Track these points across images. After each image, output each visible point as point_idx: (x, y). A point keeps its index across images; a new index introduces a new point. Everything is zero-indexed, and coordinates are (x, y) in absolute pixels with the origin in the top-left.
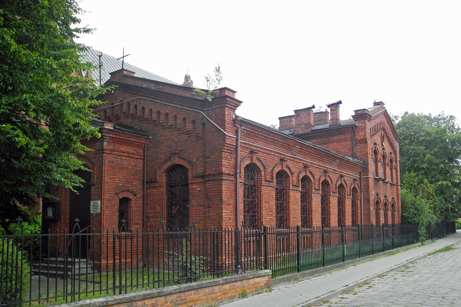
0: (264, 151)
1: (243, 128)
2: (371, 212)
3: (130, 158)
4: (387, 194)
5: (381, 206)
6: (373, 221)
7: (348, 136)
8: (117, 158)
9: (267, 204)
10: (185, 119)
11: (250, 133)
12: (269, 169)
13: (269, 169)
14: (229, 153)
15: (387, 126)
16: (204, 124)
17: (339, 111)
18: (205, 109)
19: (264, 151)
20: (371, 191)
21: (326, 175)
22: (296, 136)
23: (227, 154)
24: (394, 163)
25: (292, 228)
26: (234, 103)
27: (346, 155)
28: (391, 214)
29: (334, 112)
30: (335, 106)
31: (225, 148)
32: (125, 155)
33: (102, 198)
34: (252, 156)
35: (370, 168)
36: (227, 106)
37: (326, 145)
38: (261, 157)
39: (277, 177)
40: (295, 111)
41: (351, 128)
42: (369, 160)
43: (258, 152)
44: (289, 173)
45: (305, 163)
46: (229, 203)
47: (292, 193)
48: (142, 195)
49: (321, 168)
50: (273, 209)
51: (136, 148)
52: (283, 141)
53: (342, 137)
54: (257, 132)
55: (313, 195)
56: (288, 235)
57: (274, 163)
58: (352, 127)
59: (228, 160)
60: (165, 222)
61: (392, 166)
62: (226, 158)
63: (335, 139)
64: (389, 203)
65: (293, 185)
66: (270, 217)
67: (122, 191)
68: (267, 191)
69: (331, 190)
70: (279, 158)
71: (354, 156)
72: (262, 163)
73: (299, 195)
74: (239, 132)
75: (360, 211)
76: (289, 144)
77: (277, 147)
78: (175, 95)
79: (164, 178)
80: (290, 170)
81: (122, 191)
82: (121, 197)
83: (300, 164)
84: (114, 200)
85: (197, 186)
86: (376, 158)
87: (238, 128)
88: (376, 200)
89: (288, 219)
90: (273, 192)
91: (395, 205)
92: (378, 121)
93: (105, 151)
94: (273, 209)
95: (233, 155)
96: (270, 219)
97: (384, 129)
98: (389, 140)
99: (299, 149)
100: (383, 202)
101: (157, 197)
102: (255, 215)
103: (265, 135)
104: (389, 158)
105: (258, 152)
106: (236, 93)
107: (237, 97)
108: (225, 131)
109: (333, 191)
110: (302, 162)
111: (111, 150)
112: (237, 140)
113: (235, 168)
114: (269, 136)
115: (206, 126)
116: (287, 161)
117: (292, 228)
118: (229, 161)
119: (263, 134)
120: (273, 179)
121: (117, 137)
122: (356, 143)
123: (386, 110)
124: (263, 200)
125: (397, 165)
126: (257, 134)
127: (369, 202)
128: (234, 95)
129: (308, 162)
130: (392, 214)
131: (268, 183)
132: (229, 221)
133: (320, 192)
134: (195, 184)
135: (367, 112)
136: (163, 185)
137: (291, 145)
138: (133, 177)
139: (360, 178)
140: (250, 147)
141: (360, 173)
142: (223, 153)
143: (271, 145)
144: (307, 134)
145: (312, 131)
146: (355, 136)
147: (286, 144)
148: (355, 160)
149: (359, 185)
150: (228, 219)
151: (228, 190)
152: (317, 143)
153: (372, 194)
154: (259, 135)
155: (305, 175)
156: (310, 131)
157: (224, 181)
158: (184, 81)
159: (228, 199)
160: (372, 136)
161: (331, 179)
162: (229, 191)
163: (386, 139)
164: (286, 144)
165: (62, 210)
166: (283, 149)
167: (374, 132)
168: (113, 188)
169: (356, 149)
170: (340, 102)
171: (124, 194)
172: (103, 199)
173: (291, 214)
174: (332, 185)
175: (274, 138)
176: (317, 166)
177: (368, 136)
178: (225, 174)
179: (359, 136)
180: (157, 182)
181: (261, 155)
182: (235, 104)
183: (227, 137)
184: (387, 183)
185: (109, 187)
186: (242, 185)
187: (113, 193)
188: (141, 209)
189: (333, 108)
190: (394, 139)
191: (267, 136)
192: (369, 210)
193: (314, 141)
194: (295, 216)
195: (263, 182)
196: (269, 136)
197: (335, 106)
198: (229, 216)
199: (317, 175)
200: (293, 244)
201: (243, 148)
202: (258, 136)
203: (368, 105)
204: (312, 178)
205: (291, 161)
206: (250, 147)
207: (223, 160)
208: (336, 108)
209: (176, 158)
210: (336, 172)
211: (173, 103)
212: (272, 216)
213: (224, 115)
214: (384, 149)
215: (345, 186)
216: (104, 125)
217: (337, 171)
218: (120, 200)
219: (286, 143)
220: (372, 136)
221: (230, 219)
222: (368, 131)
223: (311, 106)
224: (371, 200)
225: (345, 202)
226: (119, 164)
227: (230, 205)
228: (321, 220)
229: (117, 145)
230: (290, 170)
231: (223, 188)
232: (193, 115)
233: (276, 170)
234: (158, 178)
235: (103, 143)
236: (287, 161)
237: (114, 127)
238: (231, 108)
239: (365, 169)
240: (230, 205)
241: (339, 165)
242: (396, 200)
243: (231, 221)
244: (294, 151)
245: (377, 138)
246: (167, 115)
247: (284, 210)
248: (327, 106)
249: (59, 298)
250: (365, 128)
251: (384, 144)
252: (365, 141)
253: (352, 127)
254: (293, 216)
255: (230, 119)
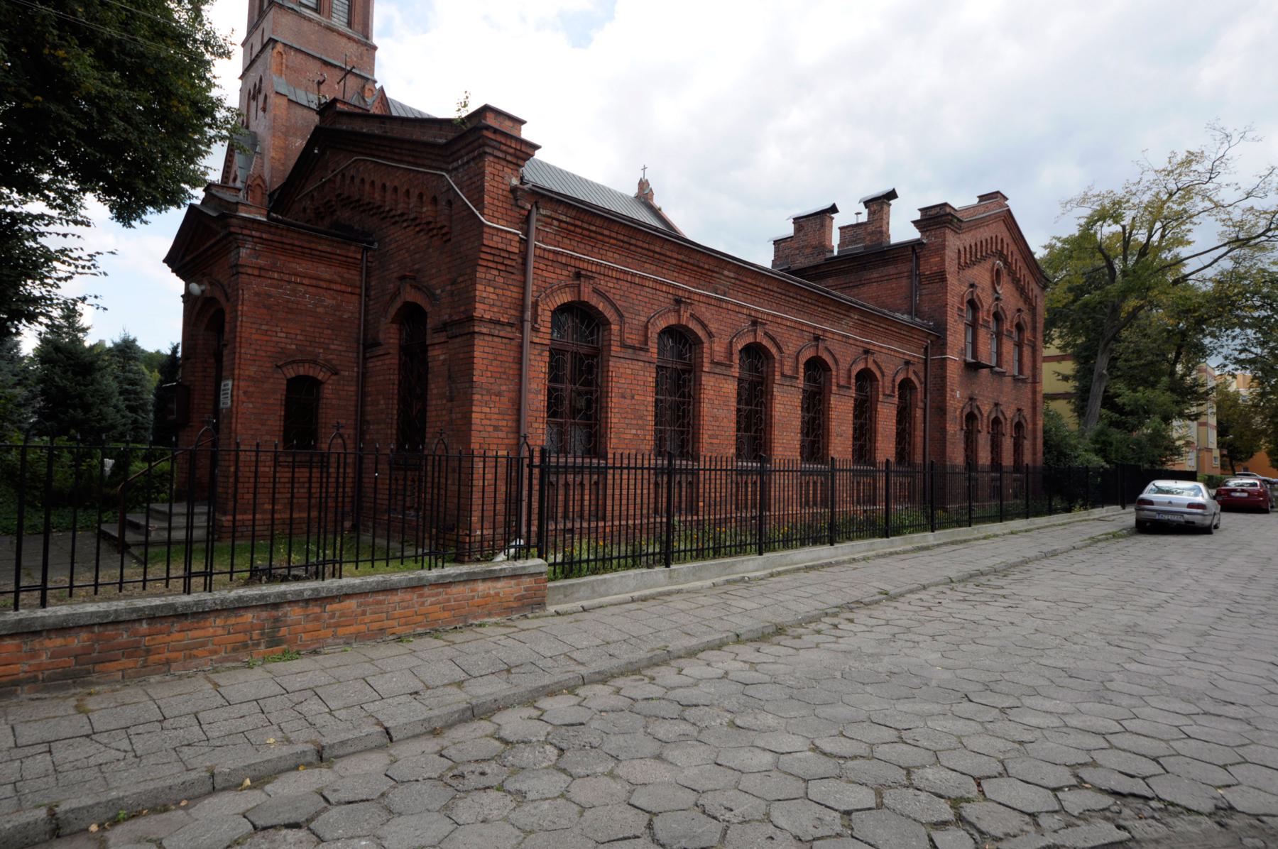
0: (622, 276)
1: (543, 212)
2: (948, 437)
3: (320, 290)
4: (1003, 399)
5: (983, 427)
6: (956, 455)
7: (904, 268)
8: (281, 287)
9: (628, 401)
10: (421, 196)
11: (572, 228)
12: (844, 366)
13: (844, 366)
14: (500, 270)
15: (1013, 247)
16: (450, 203)
17: (888, 213)
18: (450, 167)
19: (622, 276)
20: (952, 390)
21: (817, 346)
22: (794, 273)
23: (496, 273)
24: (1028, 334)
25: (708, 459)
26: (510, 147)
27: (898, 311)
28: (1012, 445)
29: (876, 217)
30: (880, 203)
31: (483, 256)
32: (306, 281)
33: (233, 375)
34: (579, 285)
35: (950, 339)
36: (490, 154)
37: (855, 291)
38: (613, 291)
39: (899, 389)
40: (797, 220)
41: (910, 249)
42: (950, 321)
43: (596, 275)
44: (701, 333)
45: (753, 313)
46: (496, 388)
47: (708, 382)
48: (355, 374)
49: (805, 328)
50: (645, 413)
51: (340, 269)
52: (680, 257)
53: (891, 270)
54: (593, 228)
55: (705, 379)
56: (693, 474)
57: (656, 307)
58: (914, 250)
59: (495, 288)
60: (394, 432)
61: (1023, 340)
62: (489, 283)
63: (875, 275)
64: (1006, 419)
65: (712, 362)
66: (634, 431)
67: (294, 362)
68: (629, 371)
69: (834, 380)
70: (670, 296)
71: (914, 311)
72: (613, 305)
73: (731, 387)
74: (534, 224)
75: (922, 434)
76: (701, 264)
77: (664, 271)
78: (403, 141)
79: (392, 336)
80: (704, 326)
81: (294, 362)
82: (291, 373)
83: (740, 315)
84: (271, 380)
85: (439, 352)
86: (975, 319)
87: (530, 212)
88: (967, 410)
89: (696, 439)
90: (647, 374)
91: (1025, 424)
92: (984, 234)
93: (241, 270)
94: (645, 413)
95: (513, 277)
96: (636, 435)
97: (1000, 255)
98: (1016, 281)
99: (733, 281)
100: (988, 417)
101: (381, 378)
102: (688, 431)
103: (621, 237)
104: (1012, 322)
105: (596, 275)
106: (523, 127)
107: (526, 133)
108: (483, 214)
109: (883, 391)
110: (745, 311)
111: (260, 269)
112: (524, 242)
113: (519, 308)
114: (633, 241)
115: (454, 206)
116: (691, 304)
117: (708, 459)
118: (500, 292)
119: (614, 235)
120: (797, 373)
121: (276, 238)
122: (920, 283)
123: (1009, 211)
124: (615, 390)
125: (1035, 337)
126: (595, 232)
127: (945, 414)
128: (520, 130)
129: (762, 312)
130: (1015, 444)
131: (630, 351)
132: (496, 434)
133: (853, 393)
134: (437, 347)
135: (948, 210)
136: (391, 351)
137: (706, 266)
138: (330, 332)
139: (926, 360)
140: (573, 262)
141: (926, 349)
142: (479, 269)
143: (647, 265)
144: (816, 267)
145: (826, 260)
146: (918, 266)
147: (691, 264)
148: (917, 319)
149: (922, 375)
150: (491, 429)
151: (496, 359)
152: (835, 287)
153: (953, 397)
154: (602, 235)
155: (752, 340)
156: (822, 262)
157: (482, 337)
158: (636, 191)
159: (492, 380)
160: (962, 267)
161: (833, 356)
162: (495, 363)
163: (1005, 278)
164: (691, 264)
165: (196, 402)
166: (687, 278)
167: (970, 259)
168: (269, 354)
169: (920, 295)
170: (892, 195)
171: (291, 371)
172: (236, 377)
173: (706, 427)
174: (838, 370)
175: (652, 247)
176: (793, 325)
177: (951, 267)
178: (481, 319)
179: (928, 267)
180: (380, 344)
181: (612, 285)
182: (515, 149)
183: (486, 230)
184: (1002, 374)
185: (256, 350)
186: (543, 351)
187: (269, 365)
188: (353, 403)
189: (875, 207)
190: (1029, 278)
191: (626, 239)
192: (943, 430)
193: (830, 281)
194: (717, 433)
195: (613, 348)
196: (633, 241)
197: (880, 203)
198: (494, 423)
199: (790, 345)
200: (707, 495)
201: (550, 263)
202: (599, 237)
203: (962, 199)
204: (774, 350)
205: (711, 307)
206: (573, 262)
207: (479, 287)
208: (882, 208)
209: (408, 288)
210: (851, 341)
211: (423, 166)
212: (641, 428)
213: (483, 174)
214: (997, 299)
215: (878, 374)
216: (237, 210)
217: (856, 340)
218: (288, 380)
219: (691, 261)
220: (962, 267)
221: (496, 428)
222: (950, 253)
223: (827, 205)
224: (950, 409)
225: (876, 411)
226: (288, 301)
227: (499, 394)
228: (798, 446)
229: (281, 257)
230: (704, 326)
231: (476, 354)
232: (435, 183)
233: (899, 379)
234: (381, 336)
235: (239, 253)
236: (691, 304)
237: (268, 216)
238: (505, 159)
239: (938, 339)
240: (499, 394)
241: (863, 327)
242: (1027, 412)
243: (501, 435)
244: (719, 283)
245: (981, 274)
246: (395, 189)
247: (684, 418)
248: (862, 204)
249: (220, 577)
250: (944, 247)
251: (998, 288)
252: (941, 277)
253: (913, 247)
254: (710, 433)
255: (504, 187)
